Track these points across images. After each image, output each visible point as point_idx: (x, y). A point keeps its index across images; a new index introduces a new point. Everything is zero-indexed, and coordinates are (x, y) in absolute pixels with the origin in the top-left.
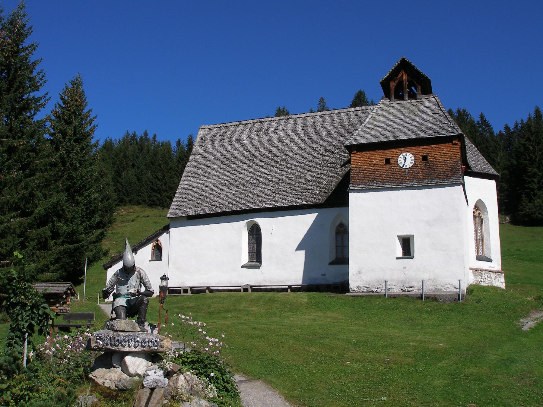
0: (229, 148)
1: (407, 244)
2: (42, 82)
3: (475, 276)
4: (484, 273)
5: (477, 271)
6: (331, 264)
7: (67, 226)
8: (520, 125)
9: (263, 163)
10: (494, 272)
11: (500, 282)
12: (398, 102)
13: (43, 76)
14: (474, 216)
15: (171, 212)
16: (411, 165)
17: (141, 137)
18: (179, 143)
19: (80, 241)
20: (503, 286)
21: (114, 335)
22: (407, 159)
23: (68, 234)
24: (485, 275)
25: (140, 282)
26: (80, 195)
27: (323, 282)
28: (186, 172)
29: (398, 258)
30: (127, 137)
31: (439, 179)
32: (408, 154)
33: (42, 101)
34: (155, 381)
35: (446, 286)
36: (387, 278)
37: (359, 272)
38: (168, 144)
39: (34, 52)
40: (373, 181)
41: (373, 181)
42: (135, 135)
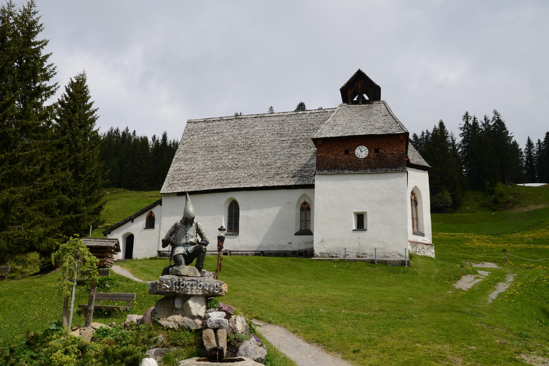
0: (212, 139)
1: (361, 219)
2: (52, 73)
3: (412, 247)
4: (418, 245)
5: (415, 244)
6: (297, 234)
7: (71, 198)
8: (425, 134)
9: (241, 152)
10: (426, 244)
11: (431, 253)
12: (354, 106)
13: (54, 69)
14: (411, 200)
15: (164, 189)
16: (366, 156)
17: (124, 132)
18: (154, 138)
19: (82, 212)
20: (433, 256)
21: (179, 280)
22: (362, 152)
23: (72, 205)
24: (420, 247)
25: (197, 233)
26: (83, 173)
27: (289, 249)
28: (176, 156)
29: (354, 230)
30: (111, 131)
31: (389, 168)
32: (363, 147)
33: (51, 90)
34: (218, 322)
35: (393, 254)
36: (346, 246)
37: (322, 241)
38: (145, 140)
39: (44, 47)
40: (335, 168)
41: (335, 168)
42: (118, 130)
